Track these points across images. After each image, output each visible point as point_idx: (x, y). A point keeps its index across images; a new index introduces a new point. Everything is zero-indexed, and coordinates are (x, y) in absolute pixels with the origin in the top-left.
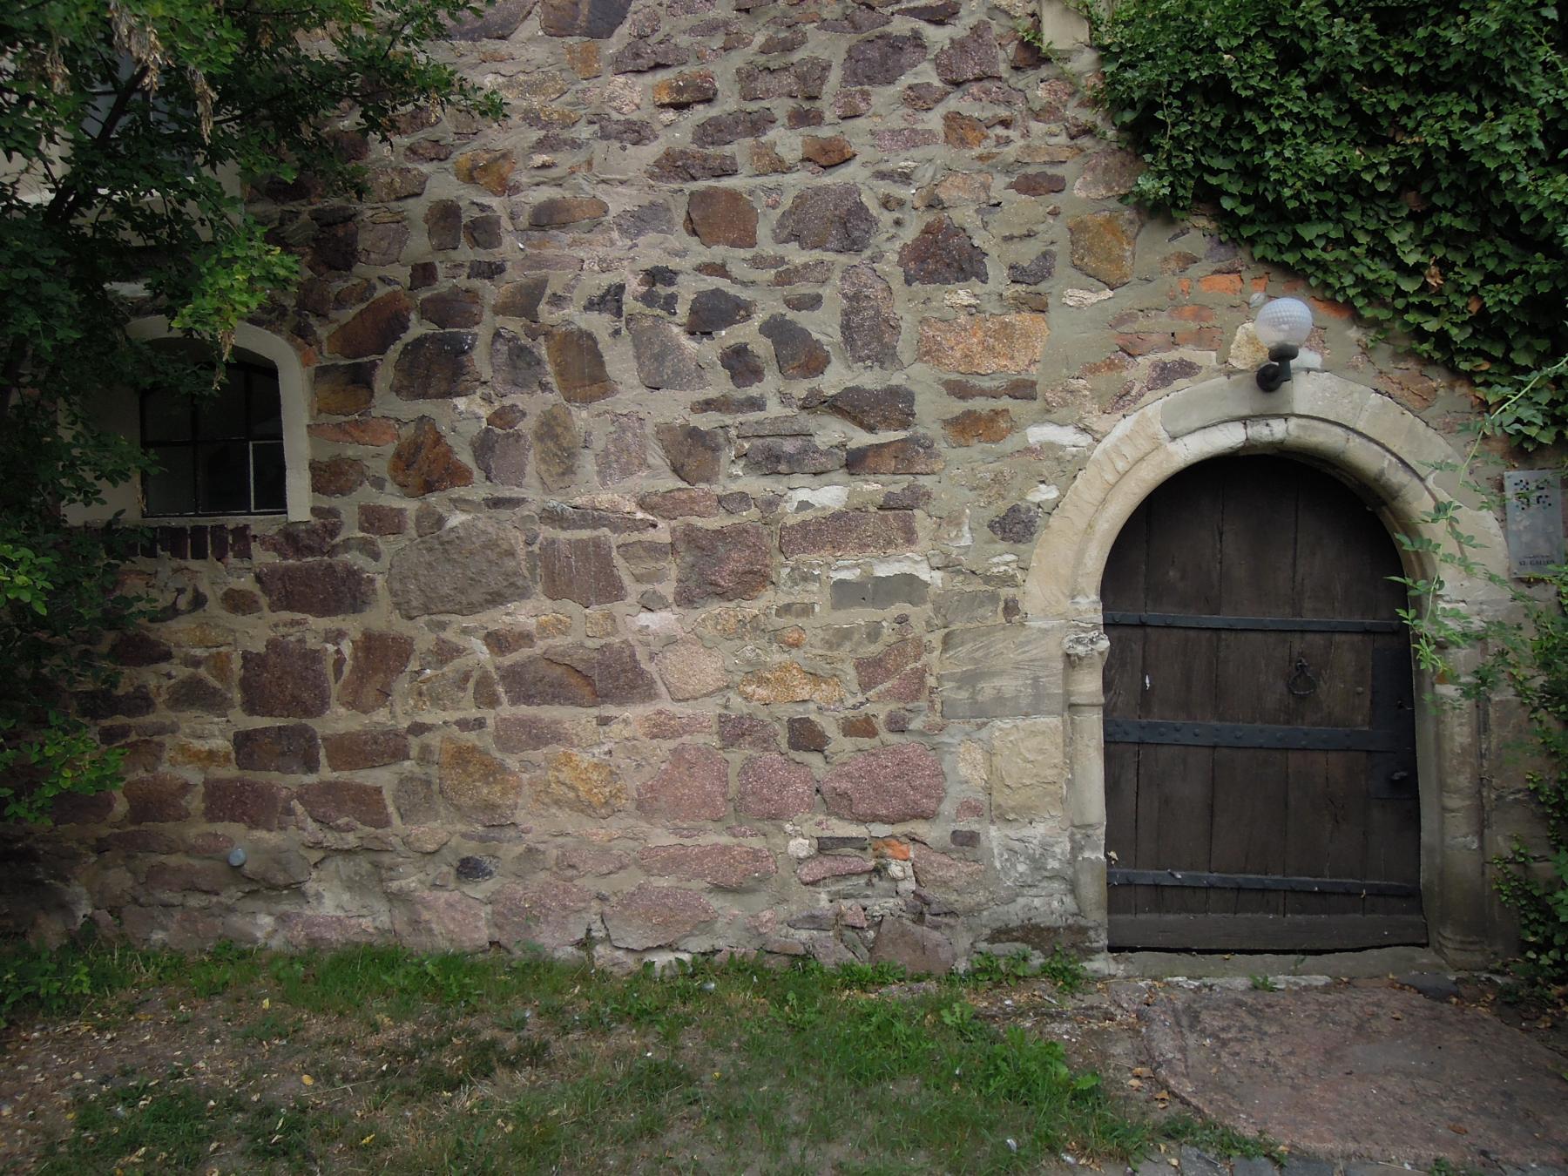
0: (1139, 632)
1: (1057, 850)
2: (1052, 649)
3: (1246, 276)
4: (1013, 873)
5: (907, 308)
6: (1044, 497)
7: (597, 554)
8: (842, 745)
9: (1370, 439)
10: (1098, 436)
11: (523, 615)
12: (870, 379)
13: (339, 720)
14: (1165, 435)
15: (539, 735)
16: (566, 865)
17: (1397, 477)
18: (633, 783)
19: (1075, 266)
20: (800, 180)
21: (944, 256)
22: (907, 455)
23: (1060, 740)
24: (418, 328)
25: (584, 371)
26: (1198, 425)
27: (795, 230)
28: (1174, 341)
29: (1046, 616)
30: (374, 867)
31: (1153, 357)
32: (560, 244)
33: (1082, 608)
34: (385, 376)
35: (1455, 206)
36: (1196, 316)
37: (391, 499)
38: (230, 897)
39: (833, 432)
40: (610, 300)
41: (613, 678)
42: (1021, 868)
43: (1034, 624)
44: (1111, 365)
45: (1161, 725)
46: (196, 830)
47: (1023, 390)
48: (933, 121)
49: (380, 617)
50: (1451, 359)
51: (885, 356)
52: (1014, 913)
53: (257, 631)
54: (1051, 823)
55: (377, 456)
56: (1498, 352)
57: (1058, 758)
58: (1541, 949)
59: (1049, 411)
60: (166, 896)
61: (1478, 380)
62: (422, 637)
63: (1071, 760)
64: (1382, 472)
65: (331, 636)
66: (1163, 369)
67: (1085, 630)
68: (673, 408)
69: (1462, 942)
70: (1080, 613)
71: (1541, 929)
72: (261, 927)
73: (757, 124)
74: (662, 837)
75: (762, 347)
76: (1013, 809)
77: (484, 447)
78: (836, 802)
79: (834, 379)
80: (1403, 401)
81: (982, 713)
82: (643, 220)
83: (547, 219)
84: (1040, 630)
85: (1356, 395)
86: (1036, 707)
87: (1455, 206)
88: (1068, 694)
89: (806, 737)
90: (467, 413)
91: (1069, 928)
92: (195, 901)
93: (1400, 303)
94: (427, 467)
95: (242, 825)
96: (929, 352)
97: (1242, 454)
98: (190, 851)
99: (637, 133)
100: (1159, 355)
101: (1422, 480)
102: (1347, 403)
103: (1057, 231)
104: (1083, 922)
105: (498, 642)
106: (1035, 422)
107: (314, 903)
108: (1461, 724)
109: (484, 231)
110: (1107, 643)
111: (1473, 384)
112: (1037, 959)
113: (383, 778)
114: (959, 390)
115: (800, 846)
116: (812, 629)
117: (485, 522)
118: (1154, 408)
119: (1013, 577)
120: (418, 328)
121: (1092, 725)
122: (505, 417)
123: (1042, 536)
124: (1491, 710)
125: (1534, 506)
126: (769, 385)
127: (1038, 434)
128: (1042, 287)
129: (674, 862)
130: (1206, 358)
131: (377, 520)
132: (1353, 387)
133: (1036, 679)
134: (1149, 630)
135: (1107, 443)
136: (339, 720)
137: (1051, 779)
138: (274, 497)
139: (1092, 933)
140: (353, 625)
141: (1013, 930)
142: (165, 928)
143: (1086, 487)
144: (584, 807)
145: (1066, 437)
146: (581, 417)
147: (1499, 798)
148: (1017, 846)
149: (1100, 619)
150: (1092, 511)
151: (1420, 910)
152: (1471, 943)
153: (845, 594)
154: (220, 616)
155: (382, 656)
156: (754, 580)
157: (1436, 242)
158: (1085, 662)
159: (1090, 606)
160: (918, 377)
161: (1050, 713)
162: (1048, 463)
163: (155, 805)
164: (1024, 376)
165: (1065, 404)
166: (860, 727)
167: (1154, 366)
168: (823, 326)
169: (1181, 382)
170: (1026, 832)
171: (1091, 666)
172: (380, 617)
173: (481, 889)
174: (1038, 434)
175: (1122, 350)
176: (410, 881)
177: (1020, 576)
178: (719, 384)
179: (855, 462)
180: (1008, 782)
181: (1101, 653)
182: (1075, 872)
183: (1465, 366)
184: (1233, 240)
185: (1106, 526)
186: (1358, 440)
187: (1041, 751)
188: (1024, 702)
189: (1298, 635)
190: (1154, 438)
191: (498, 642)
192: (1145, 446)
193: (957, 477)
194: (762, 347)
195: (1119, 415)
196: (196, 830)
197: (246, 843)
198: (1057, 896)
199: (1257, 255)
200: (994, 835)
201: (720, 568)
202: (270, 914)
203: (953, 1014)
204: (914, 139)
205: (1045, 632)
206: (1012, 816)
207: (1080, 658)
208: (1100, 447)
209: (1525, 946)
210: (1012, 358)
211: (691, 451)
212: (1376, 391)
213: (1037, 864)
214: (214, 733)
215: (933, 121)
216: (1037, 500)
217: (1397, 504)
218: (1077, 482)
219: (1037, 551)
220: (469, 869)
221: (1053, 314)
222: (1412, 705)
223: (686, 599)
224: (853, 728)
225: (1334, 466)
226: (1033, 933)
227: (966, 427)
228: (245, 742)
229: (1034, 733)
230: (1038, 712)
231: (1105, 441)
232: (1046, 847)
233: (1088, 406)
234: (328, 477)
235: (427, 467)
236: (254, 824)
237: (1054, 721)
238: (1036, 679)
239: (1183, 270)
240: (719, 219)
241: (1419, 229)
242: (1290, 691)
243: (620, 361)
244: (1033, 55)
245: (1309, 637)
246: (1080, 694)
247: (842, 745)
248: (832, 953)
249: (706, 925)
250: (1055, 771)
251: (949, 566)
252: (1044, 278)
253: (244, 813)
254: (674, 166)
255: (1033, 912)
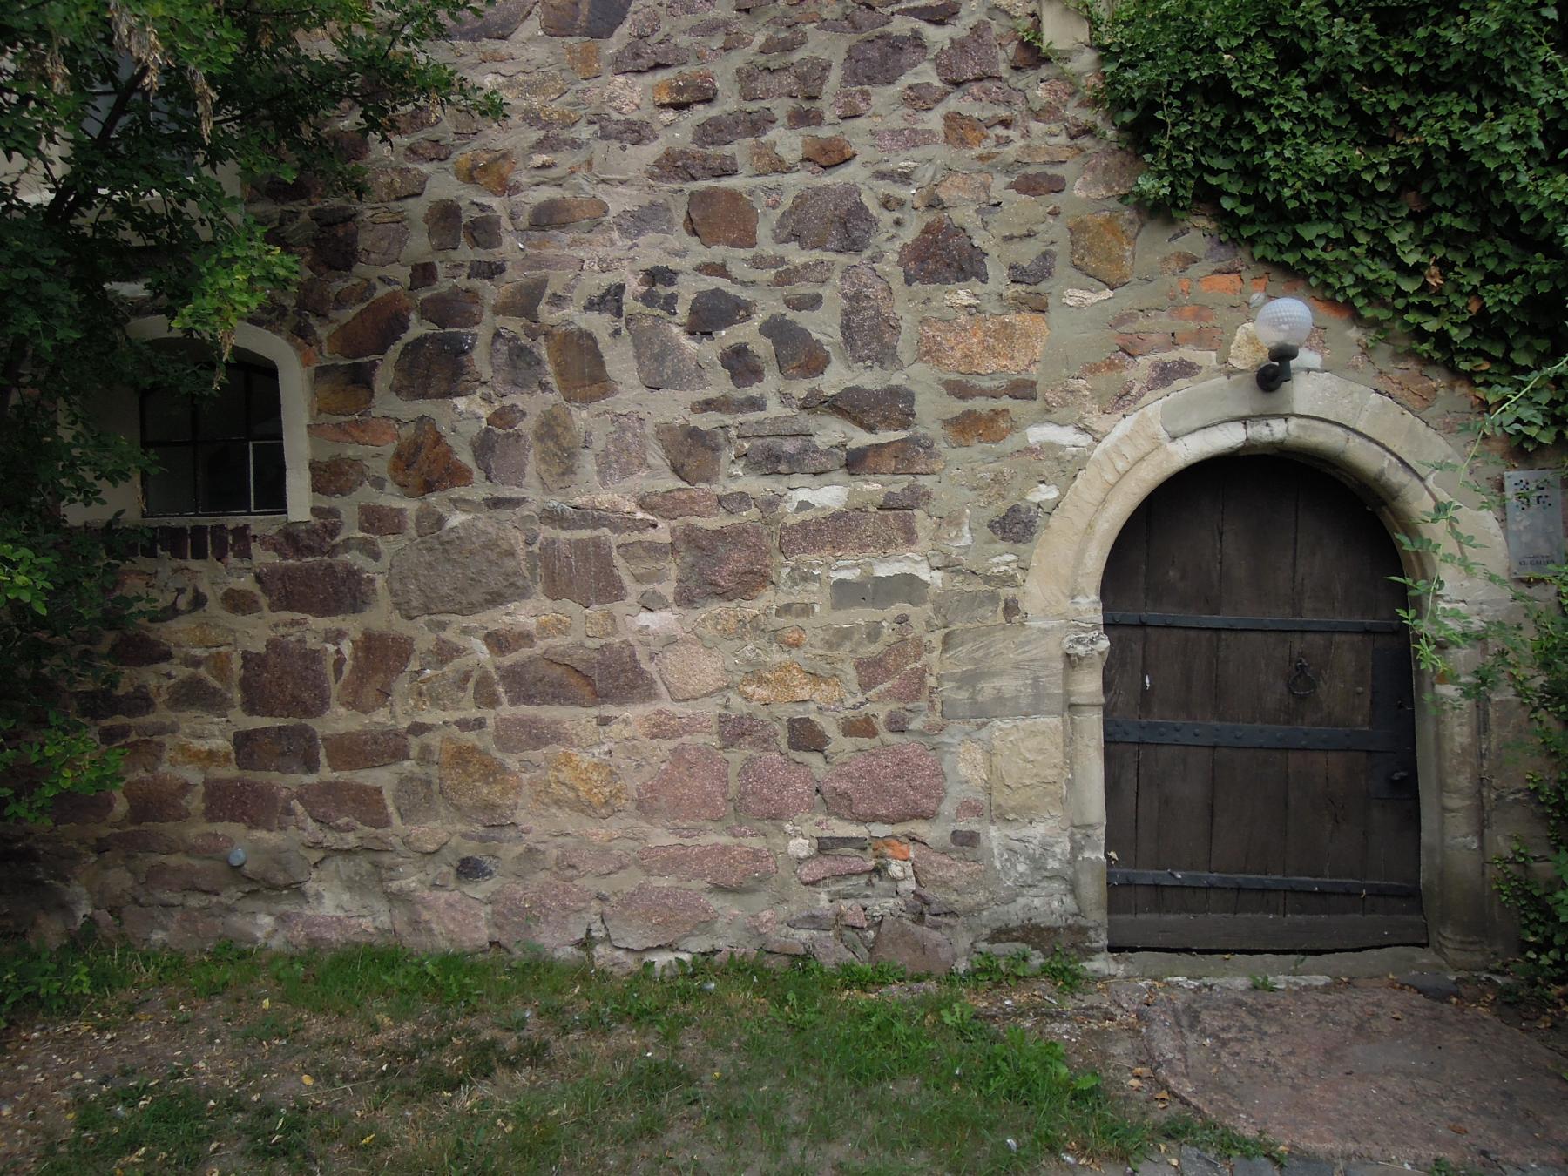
0: (1139, 632)
1: (1057, 850)
2: (1052, 649)
3: (1246, 276)
4: (1013, 873)
5: (907, 308)
6: (1044, 497)
7: (597, 554)
8: (842, 745)
9: (1370, 439)
10: (1098, 436)
11: (523, 615)
12: (870, 379)
13: (339, 720)
14: (1165, 435)
15: (539, 735)
16: (566, 865)
17: (1397, 477)
18: (633, 783)
19: (1075, 266)
20: (800, 180)
21: (944, 256)
22: (907, 455)
23: (1060, 740)
24: (418, 328)
25: (584, 371)
26: (1198, 425)
27: (795, 230)
28: (1174, 341)
29: (1046, 616)
30: (374, 867)
31: (1153, 357)
32: (560, 244)
33: (1082, 608)
34: (385, 376)
35: (1455, 206)
36: (1196, 316)
37: (391, 499)
38: (230, 897)
39: (833, 432)
40: (610, 300)
41: (613, 678)
42: (1021, 868)
43: (1034, 624)
44: (1111, 365)
45: (1161, 725)
46: (196, 830)
47: (1023, 390)
48: (933, 121)
49: (380, 617)
50: (1451, 359)
51: (885, 356)
52: (1014, 913)
53: (257, 631)
54: (1051, 823)
55: (377, 456)
56: (1498, 352)
57: (1058, 758)
58: (1541, 949)
59: (1049, 411)
60: (166, 896)
61: (1478, 380)
62: (422, 637)
63: (1071, 760)
64: (1382, 472)
65: (331, 636)
66: (1163, 369)
67: (1085, 630)
68: (673, 408)
69: (1462, 942)
70: (1080, 613)
71: (1541, 929)
72: (261, 927)
73: (757, 124)
74: (662, 837)
75: (762, 347)
76: (1013, 809)
77: (484, 447)
78: (836, 802)
79: (834, 379)
80: (1403, 401)
81: (982, 713)
82: (643, 220)
83: (547, 219)
84: (1040, 630)
85: (1356, 395)
86: (1036, 707)
87: (1455, 206)
88: (1068, 694)
89: (806, 737)
90: (467, 413)
91: (1069, 928)
92: (195, 901)
93: (1400, 303)
94: (427, 467)
95: (242, 825)
96: (929, 352)
97: (1242, 454)
98: (190, 851)
99: (637, 133)
100: (1159, 355)
101: (1422, 480)
102: (1347, 403)
103: (1057, 231)
104: (1083, 922)
105: (498, 642)
106: (1035, 422)
107: (314, 903)
108: (1461, 724)
109: (484, 231)
110: (1107, 643)
111: (1473, 384)
112: (1037, 959)
113: (383, 778)
114: (959, 390)
115: (800, 846)
116: (812, 629)
117: (485, 522)
118: (1154, 408)
119: (1013, 577)
120: (418, 328)
121: (1092, 725)
122: (505, 417)
123: (1042, 536)
124: (1491, 710)
125: (1534, 506)
126: (769, 385)
127: (1038, 434)
128: (1042, 287)
129: (674, 862)
130: (1206, 358)
131: (377, 520)
132: (1353, 387)
133: (1036, 679)
134: (1149, 630)
135: (1107, 443)
136: (339, 720)
137: (1051, 779)
138: (274, 497)
139: (1092, 933)
140: (353, 625)
141: (1013, 930)
142: (165, 928)
143: (1086, 487)
144: (584, 807)
145: (1066, 437)
146: (581, 417)
147: (1499, 798)
148: (1017, 846)
149: (1100, 619)
150: (1092, 511)
151: (1420, 910)
152: (1471, 943)
153: (845, 594)
154: (220, 616)
155: (382, 656)
156: (754, 580)
157: (1436, 242)
158: (1085, 662)
159: (1090, 606)
160: (918, 377)
161: (1050, 713)
162: (1048, 463)
163: (155, 805)
164: (1024, 376)
165: (1065, 404)
166: (860, 727)
167: (1154, 366)
168: (823, 326)
169: (1181, 382)
170: (1026, 832)
171: (1091, 666)
172: (380, 617)
173: (481, 889)
174: (1038, 434)
175: (1122, 350)
176: (410, 881)
177: (1020, 576)
178: (719, 384)
179: (855, 462)
180: (1008, 782)
181: (1101, 653)
182: (1075, 872)
183: (1465, 366)
184: (1233, 240)
185: (1106, 526)
186: (1358, 440)
187: (1041, 751)
188: (1024, 702)
189: (1298, 635)
190: (1154, 438)
191: (498, 642)
192: (1145, 446)
193: (957, 477)
194: (762, 347)
195: (1119, 415)
196: (196, 830)
197: (246, 843)
198: (1057, 896)
199: (1257, 255)
200: (994, 835)
201: (720, 568)
202: (270, 914)
203: (953, 1014)
204: (914, 139)
205: (1045, 632)
206: (1012, 816)
207: (1080, 658)
208: (1100, 447)
209: (1525, 946)
210: (1012, 358)
211: (691, 451)
212: (1376, 391)
213: (1037, 864)
214: (214, 733)
215: (933, 121)
216: (1037, 500)
217: (1397, 504)
218: (1077, 482)
219: (1037, 551)
220: (469, 869)
221: (1053, 314)
222: (1412, 705)
223: (686, 599)
224: (853, 728)
225: (1334, 466)
226: (1033, 933)
227: (966, 427)
228: (245, 742)
229: (1034, 733)
230: (1038, 712)
231: (1105, 441)
232: (1046, 847)
233: (1088, 406)
234: (328, 477)
235: (427, 467)
236: (254, 824)
237: (1054, 721)
238: (1036, 679)
239: (1183, 270)
240: (719, 219)
241: (1419, 229)
242: (1290, 691)
243: (620, 361)
244: (1033, 55)
245: (1309, 637)
246: (1080, 694)
247: (842, 745)
248: (832, 953)
249: (706, 925)
250: (1055, 771)
251: (949, 566)
252: (1044, 278)
253: (244, 813)
254: (674, 166)
255: (1033, 912)
